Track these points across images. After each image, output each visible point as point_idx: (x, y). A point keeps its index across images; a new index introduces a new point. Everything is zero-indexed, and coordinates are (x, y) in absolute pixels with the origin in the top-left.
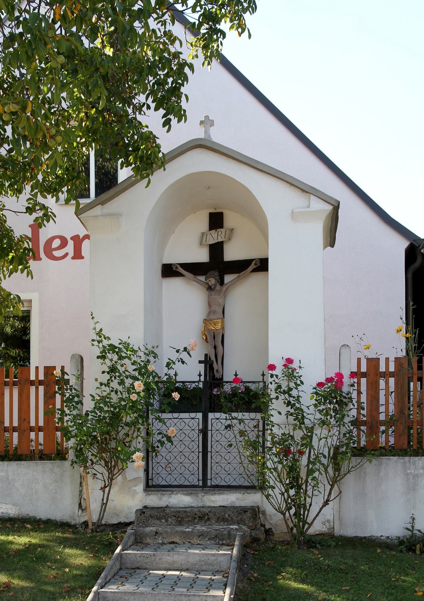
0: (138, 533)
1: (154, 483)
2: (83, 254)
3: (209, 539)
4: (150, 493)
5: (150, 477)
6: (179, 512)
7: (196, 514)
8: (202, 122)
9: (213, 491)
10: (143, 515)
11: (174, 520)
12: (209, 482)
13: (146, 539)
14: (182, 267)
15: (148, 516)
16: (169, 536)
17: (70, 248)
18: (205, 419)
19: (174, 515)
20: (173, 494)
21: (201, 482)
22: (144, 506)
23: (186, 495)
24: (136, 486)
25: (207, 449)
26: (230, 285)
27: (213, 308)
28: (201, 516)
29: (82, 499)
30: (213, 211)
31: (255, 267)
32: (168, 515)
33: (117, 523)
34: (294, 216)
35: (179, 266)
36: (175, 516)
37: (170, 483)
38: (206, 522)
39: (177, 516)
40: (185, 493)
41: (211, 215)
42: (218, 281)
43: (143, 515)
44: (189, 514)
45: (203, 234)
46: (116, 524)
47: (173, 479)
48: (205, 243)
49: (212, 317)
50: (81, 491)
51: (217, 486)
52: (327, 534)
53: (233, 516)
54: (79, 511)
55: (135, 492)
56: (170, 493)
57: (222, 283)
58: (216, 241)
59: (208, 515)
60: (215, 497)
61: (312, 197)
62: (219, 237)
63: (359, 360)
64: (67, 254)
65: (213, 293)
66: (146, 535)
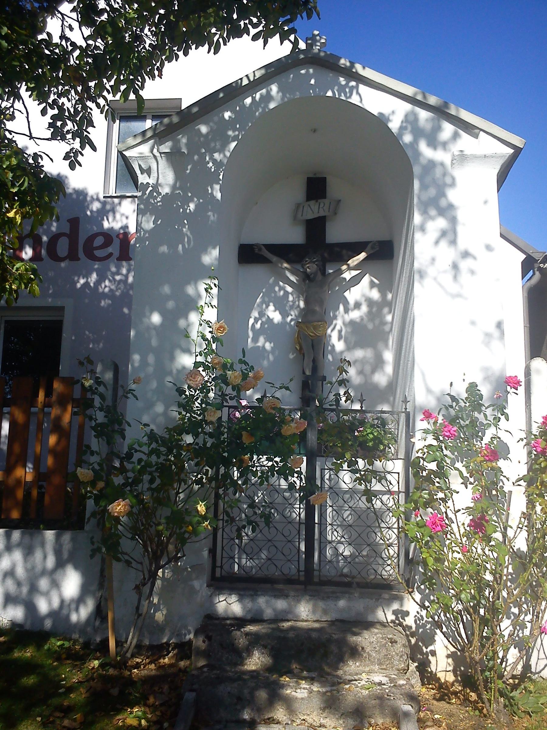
5: (218, 564)
14: (266, 248)
30: (311, 176)
35: (263, 248)
45: (298, 206)
54: (96, 619)
56: (251, 592)
57: (323, 272)
58: (316, 216)
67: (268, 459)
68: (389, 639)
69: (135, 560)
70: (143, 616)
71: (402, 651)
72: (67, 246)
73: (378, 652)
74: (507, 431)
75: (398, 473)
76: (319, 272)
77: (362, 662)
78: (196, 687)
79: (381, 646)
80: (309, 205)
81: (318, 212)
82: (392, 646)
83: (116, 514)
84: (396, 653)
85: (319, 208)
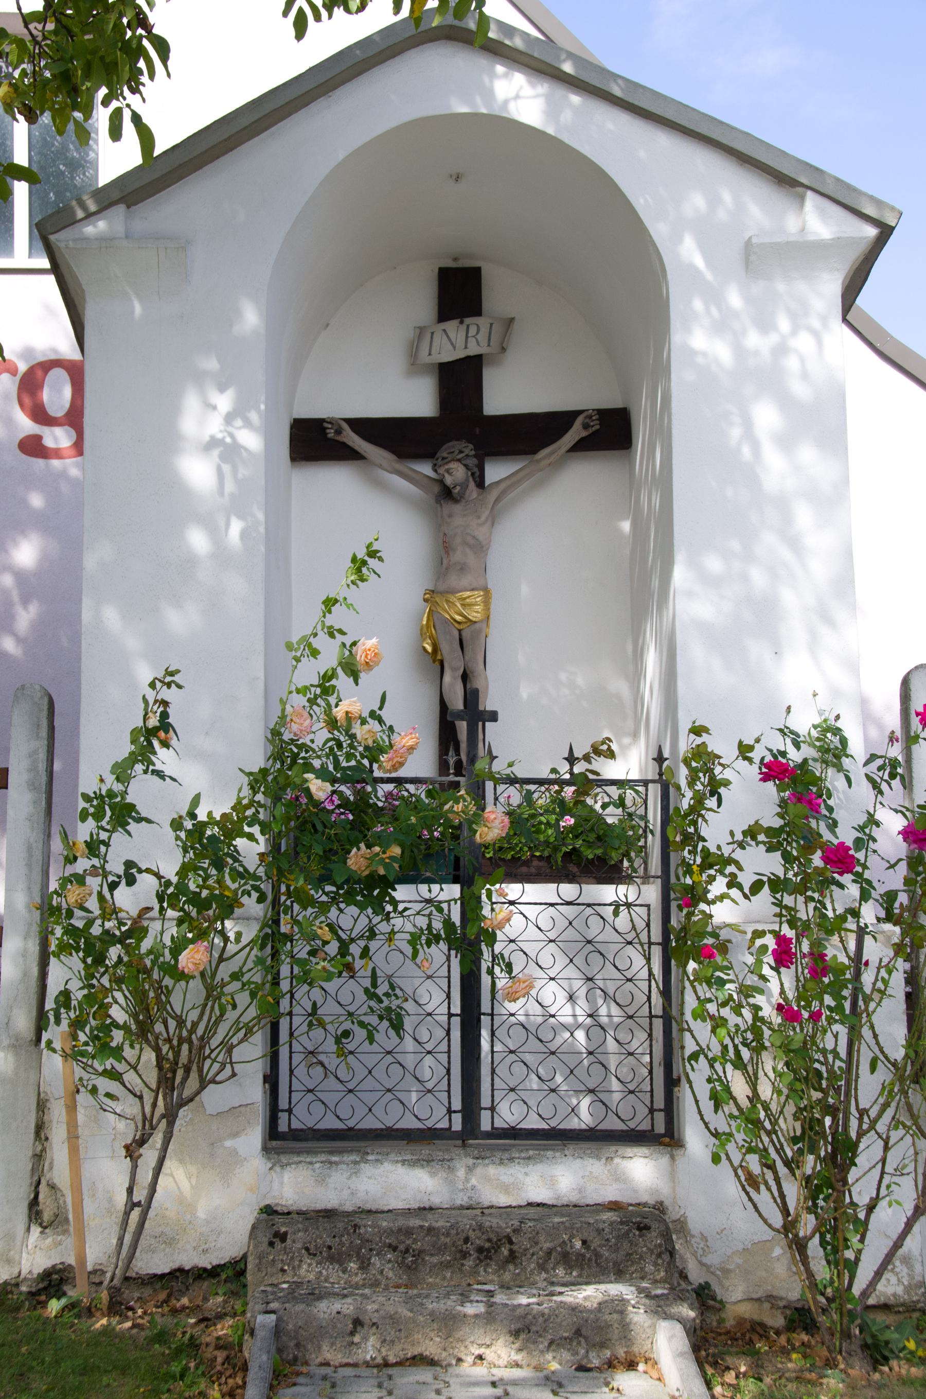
0: (290, 1327)
1: (295, 1125)
3: (551, 1343)
4: (284, 1159)
5: (283, 1103)
6: (408, 1232)
7: (466, 1240)
9: (505, 1149)
10: (279, 1245)
11: (390, 1261)
12: (485, 1116)
13: (319, 1348)
15: (300, 1249)
16: (403, 1334)
18: (658, 877)
19: (390, 1246)
20: (367, 1162)
22: (262, 1204)
23: (413, 1164)
24: (235, 1135)
25: (479, 1005)
26: (504, 493)
28: (487, 1245)
29: (43, 1188)
31: (584, 434)
32: (368, 1245)
33: (167, 1270)
35: (345, 426)
36: (395, 1249)
37: (351, 1124)
38: (503, 1266)
39: (402, 1247)
40: (409, 1157)
42: (473, 474)
43: (279, 1245)
44: (442, 1238)
45: (421, 330)
46: (163, 1276)
47: (361, 1111)
48: (427, 359)
50: (39, 1157)
51: (513, 1133)
52: (902, 1305)
53: (601, 1246)
55: (235, 1159)
58: (460, 354)
59: (511, 1242)
60: (511, 1171)
61: (811, 199)
62: (472, 343)
63: (79, 972)
65: (457, 509)
66: (321, 1332)
67: (153, 1009)
68: (634, 1224)
69: (410, 902)
70: (425, 946)
71: (660, 1245)
73: (616, 1249)
75: (648, 906)
76: (471, 479)
77: (582, 1269)
78: (274, 1305)
79: (618, 1238)
80: (444, 330)
81: (466, 347)
82: (640, 1236)
83: (367, 872)
84: (648, 1249)
85: (467, 337)
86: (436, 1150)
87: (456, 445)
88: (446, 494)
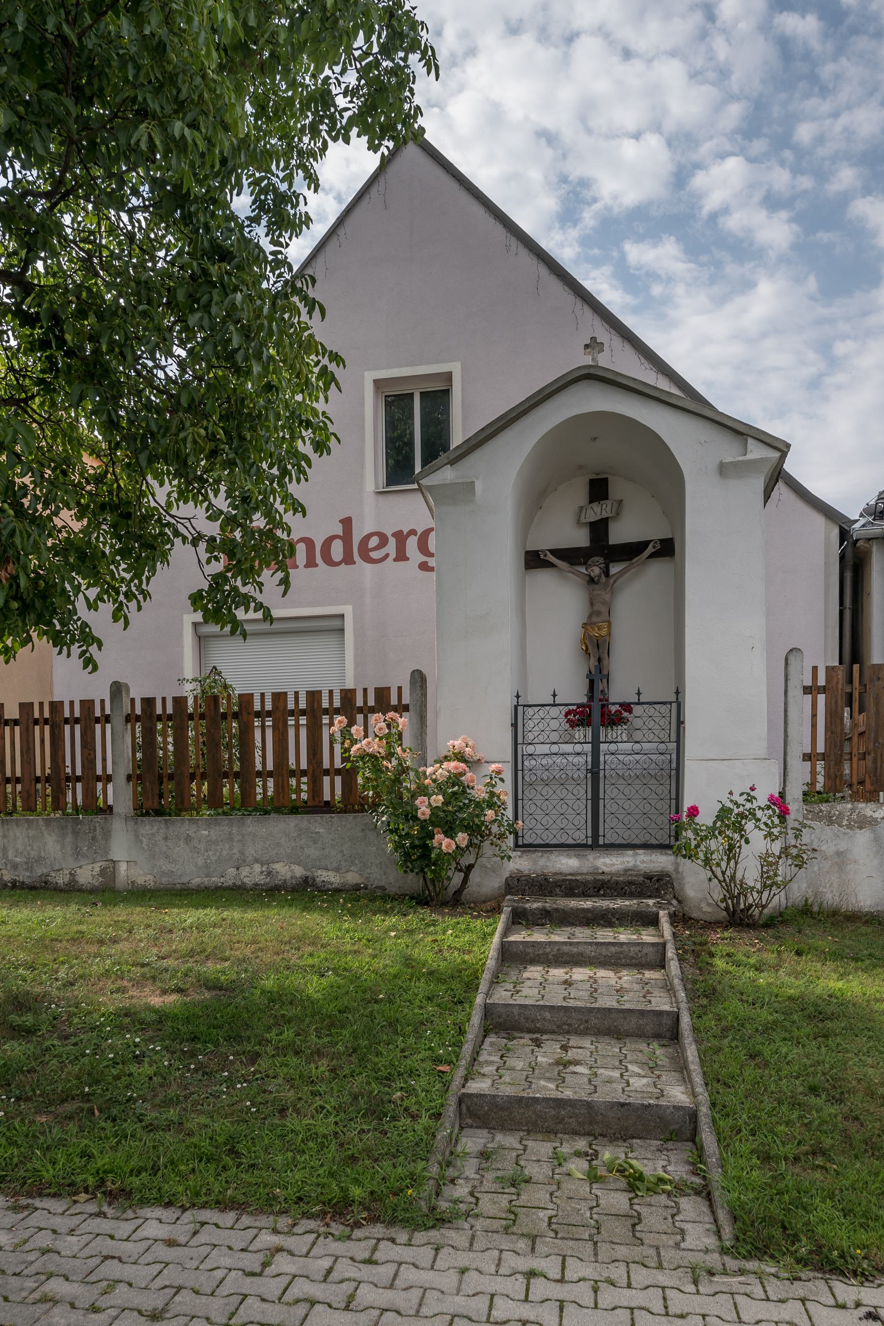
1: (526, 842)
2: (408, 555)
8: (587, 346)
17: (391, 548)
21: (590, 840)
27: (596, 608)
34: (724, 470)
41: (592, 482)
47: (551, 836)
49: (595, 619)
57: (607, 575)
61: (750, 441)
63: (815, 669)
64: (387, 556)
65: (596, 586)
72: (341, 550)
74: (647, 1287)
86: (582, 852)
87: (596, 559)
88: (592, 581)
